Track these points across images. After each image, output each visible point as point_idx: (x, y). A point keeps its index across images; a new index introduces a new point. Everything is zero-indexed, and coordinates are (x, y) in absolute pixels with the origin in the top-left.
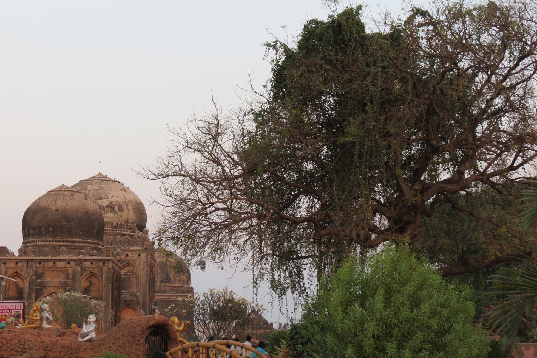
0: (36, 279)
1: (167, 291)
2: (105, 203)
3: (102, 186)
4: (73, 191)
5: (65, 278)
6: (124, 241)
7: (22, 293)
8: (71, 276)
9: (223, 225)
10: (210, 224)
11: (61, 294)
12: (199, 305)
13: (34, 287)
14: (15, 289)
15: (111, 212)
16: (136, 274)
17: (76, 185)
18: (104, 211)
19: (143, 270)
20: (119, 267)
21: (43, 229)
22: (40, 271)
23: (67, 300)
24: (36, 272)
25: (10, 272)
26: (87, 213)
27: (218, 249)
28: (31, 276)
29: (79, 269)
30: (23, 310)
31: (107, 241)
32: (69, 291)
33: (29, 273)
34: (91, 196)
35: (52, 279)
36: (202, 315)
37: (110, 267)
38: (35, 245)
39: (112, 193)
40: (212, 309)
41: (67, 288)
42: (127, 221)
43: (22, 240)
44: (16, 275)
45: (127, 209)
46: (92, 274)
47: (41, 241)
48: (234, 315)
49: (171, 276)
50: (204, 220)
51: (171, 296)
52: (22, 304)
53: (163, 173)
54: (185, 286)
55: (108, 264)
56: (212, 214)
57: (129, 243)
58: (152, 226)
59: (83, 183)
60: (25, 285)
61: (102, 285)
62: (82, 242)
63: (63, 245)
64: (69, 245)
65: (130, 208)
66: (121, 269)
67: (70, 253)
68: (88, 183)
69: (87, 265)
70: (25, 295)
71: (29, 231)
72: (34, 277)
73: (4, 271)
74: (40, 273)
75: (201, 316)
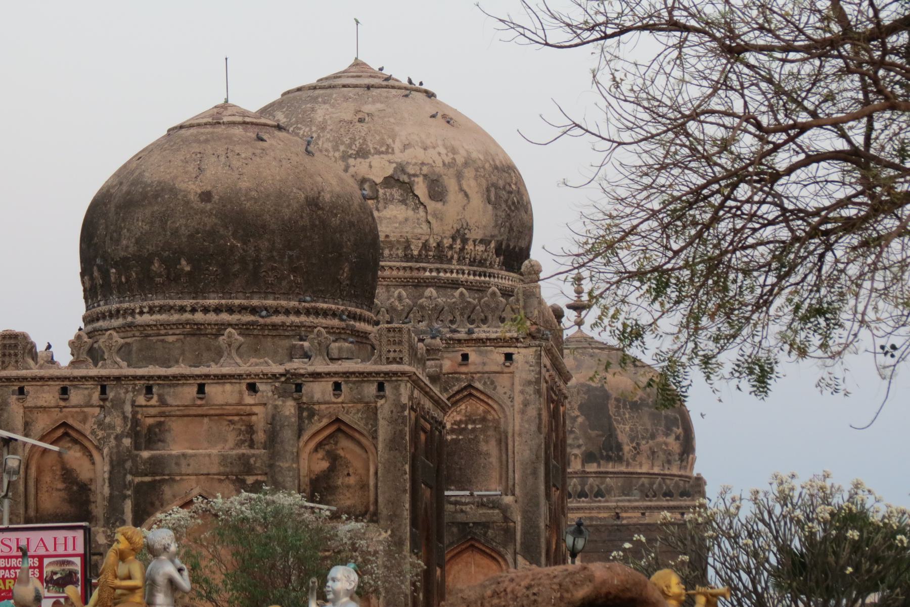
0: (137, 447)
1: (609, 490)
2: (378, 168)
3: (368, 108)
4: (260, 126)
5: (239, 444)
6: (452, 308)
7: (88, 502)
8: (260, 436)
9: (835, 220)
10: (786, 216)
11: (225, 497)
12: (737, 536)
13: (129, 477)
14: (61, 486)
15: (403, 202)
16: (496, 428)
17: (272, 105)
18: (376, 198)
19: (523, 412)
20: (437, 402)
21: (156, 266)
22: (150, 421)
23: (245, 519)
24: (136, 422)
25: (43, 423)
26: (313, 203)
27: (819, 312)
28: (118, 438)
29: (289, 408)
30: (85, 558)
31: (391, 310)
32: (256, 487)
33: (111, 427)
34: (329, 145)
35: (194, 447)
36: (749, 573)
37: (404, 400)
38: (131, 325)
39: (403, 134)
40: (784, 549)
41: (250, 480)
42: (460, 235)
43: (81, 308)
44: (65, 433)
45: (461, 190)
46: (340, 428)
47: (151, 311)
48: (869, 571)
49: (623, 438)
50: (762, 202)
51: (625, 509)
52: (80, 534)
53: (601, 19)
54: (675, 471)
55: (397, 388)
56: (793, 176)
57: (471, 316)
58: (552, 243)
59: (295, 99)
60: (96, 470)
61: (375, 464)
62: (298, 313)
63: (230, 325)
64: (253, 323)
65: (470, 184)
66: (444, 409)
67: (256, 351)
68: (314, 99)
69: (317, 396)
70: (99, 509)
71: (105, 274)
72: (127, 442)
73: (19, 422)
74: (150, 428)
75: (744, 576)
